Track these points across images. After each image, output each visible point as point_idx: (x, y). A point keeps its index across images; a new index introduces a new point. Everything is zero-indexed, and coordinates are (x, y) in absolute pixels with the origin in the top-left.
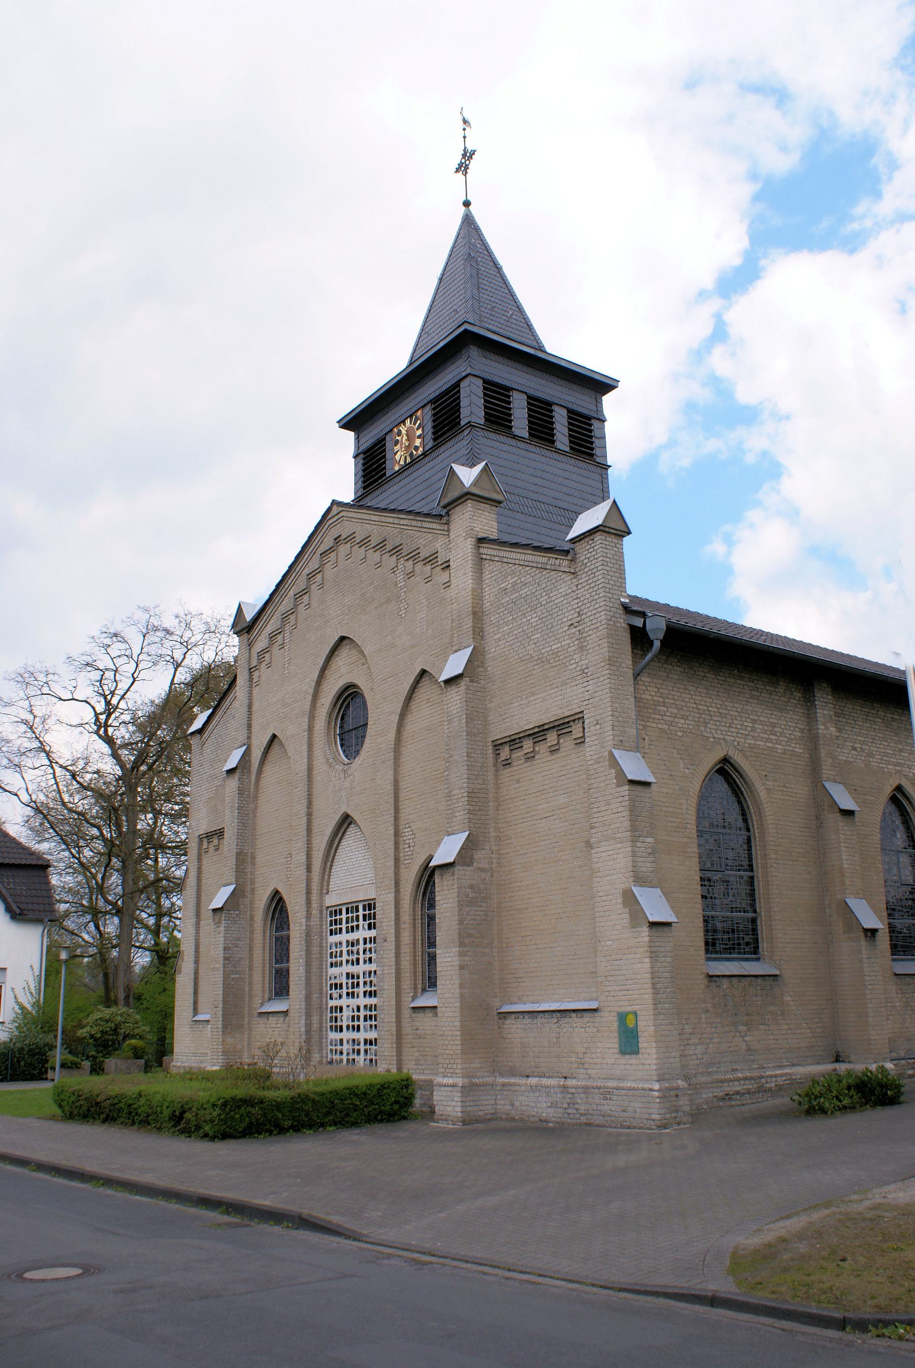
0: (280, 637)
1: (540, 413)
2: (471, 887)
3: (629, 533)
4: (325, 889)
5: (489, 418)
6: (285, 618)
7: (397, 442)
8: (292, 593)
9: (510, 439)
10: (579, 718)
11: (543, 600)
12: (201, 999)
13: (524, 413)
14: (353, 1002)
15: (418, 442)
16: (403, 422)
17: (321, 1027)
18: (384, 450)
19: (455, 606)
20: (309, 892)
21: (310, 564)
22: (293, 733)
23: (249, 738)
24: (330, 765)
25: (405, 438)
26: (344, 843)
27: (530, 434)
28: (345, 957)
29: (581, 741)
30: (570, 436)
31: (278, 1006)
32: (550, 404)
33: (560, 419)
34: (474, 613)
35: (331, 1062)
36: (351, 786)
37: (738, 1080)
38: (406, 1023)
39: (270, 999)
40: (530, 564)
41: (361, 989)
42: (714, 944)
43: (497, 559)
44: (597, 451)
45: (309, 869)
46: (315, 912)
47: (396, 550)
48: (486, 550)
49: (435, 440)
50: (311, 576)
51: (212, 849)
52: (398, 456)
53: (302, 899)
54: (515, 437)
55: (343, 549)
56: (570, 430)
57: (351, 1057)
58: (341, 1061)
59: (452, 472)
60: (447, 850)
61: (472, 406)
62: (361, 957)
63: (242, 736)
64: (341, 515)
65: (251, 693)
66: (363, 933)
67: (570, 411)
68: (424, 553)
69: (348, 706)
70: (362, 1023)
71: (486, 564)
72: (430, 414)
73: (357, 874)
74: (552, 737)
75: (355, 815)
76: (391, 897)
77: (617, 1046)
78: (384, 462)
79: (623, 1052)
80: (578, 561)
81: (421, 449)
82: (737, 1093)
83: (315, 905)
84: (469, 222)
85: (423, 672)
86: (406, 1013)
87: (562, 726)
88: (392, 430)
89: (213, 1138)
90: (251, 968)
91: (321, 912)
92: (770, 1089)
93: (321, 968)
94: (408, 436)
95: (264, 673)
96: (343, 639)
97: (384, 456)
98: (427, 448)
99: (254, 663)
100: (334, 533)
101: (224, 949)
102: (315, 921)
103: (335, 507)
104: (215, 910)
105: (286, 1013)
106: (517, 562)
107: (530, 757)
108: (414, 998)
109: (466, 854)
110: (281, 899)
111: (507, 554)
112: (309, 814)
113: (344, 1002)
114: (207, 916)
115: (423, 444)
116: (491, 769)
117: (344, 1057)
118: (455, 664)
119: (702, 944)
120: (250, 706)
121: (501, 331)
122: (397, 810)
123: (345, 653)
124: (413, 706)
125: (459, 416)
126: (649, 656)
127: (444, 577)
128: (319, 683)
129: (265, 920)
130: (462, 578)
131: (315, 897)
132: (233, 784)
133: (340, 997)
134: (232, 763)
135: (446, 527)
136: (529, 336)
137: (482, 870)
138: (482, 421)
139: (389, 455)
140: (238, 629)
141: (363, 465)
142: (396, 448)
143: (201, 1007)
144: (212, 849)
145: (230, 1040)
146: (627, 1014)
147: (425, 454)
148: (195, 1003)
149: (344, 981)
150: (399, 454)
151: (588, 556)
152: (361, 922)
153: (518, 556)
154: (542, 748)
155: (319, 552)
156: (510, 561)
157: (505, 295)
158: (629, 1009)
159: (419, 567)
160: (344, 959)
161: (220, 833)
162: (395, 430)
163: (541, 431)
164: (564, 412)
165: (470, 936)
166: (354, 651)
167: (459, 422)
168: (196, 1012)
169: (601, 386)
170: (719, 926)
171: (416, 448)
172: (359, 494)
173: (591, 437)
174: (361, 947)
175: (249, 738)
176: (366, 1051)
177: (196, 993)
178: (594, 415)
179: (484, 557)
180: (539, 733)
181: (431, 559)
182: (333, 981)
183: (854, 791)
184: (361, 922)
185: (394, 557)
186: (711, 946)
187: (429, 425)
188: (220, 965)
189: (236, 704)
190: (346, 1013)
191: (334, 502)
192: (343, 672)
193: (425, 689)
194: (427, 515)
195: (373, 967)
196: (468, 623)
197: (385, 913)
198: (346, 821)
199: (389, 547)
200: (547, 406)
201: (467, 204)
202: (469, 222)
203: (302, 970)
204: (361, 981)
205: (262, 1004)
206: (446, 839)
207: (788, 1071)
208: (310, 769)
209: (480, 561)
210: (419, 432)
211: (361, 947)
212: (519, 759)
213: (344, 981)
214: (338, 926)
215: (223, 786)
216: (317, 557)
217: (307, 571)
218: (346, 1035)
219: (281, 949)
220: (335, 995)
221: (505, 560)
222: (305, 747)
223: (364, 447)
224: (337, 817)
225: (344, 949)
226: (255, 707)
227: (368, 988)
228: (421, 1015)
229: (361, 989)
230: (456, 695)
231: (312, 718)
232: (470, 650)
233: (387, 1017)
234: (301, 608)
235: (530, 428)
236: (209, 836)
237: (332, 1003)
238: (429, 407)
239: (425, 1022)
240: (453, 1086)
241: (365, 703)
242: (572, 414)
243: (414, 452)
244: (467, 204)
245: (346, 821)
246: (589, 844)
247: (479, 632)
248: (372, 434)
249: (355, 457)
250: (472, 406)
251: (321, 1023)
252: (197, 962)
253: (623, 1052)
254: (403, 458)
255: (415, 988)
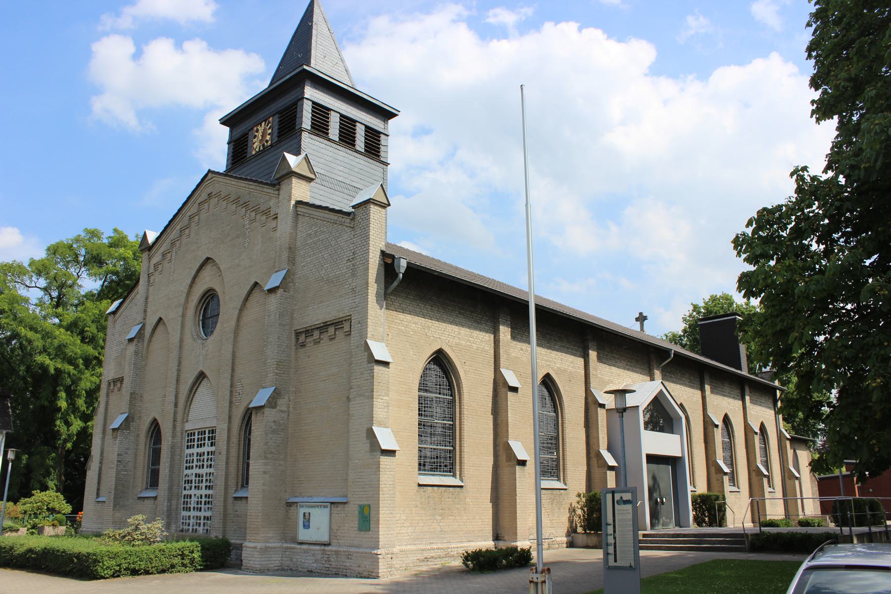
0: (169, 255)
2: (274, 422)
3: (389, 205)
4: (185, 420)
5: (313, 126)
6: (173, 244)
8: (178, 227)
10: (348, 319)
11: (333, 243)
12: (102, 488)
13: (337, 126)
14: (198, 493)
15: (268, 137)
16: (261, 124)
17: (177, 508)
19: (278, 243)
20: (175, 420)
22: (172, 317)
23: (144, 319)
24: (194, 340)
26: (199, 390)
27: (340, 139)
28: (195, 463)
29: (348, 334)
31: (151, 493)
32: (355, 121)
33: (360, 132)
34: (290, 248)
35: (182, 531)
36: (205, 353)
37: (433, 549)
38: (230, 507)
39: (146, 489)
41: (204, 484)
42: (424, 465)
44: (382, 154)
45: (176, 405)
46: (179, 434)
47: (245, 205)
48: (301, 209)
49: (278, 137)
50: (191, 218)
51: (116, 389)
52: (256, 145)
53: (170, 425)
54: (329, 140)
55: (214, 201)
58: (188, 530)
59: (284, 158)
60: (261, 398)
62: (205, 463)
63: (140, 318)
65: (148, 290)
66: (206, 449)
67: (366, 127)
68: (263, 208)
69: (209, 303)
70: (203, 506)
73: (206, 411)
74: (331, 330)
75: (207, 373)
76: (225, 426)
77: (357, 526)
79: (360, 530)
82: (432, 557)
83: (178, 429)
85: (256, 284)
86: (230, 500)
87: (337, 324)
89: (201, 570)
90: (135, 468)
91: (182, 434)
92: (453, 556)
93: (179, 470)
94: (262, 135)
95: (156, 277)
96: (208, 259)
99: (152, 270)
101: (118, 455)
102: (178, 439)
104: (114, 430)
105: (155, 498)
107: (317, 342)
108: (236, 491)
109: (272, 402)
110: (158, 424)
111: (314, 213)
112: (179, 370)
113: (193, 492)
114: (109, 432)
115: (272, 139)
116: (294, 348)
117: (191, 528)
118: (275, 280)
119: (417, 465)
120: (147, 298)
122: (233, 370)
123: (208, 269)
124: (248, 304)
126: (395, 284)
127: (273, 224)
128: (191, 286)
129: (147, 437)
130: (285, 225)
131: (178, 424)
132: (132, 348)
133: (191, 488)
134: (132, 335)
137: (282, 411)
138: (309, 128)
140: (143, 247)
143: (102, 492)
144: (116, 389)
145: (118, 514)
146: (365, 506)
147: (271, 145)
148: (98, 489)
149: (194, 479)
152: (207, 441)
153: (320, 214)
154: (325, 336)
155: (198, 202)
158: (366, 503)
159: (258, 216)
160: (194, 464)
161: (121, 380)
164: (363, 127)
165: (271, 453)
166: (215, 267)
168: (98, 495)
170: (428, 454)
171: (267, 141)
174: (206, 457)
175: (144, 319)
176: (204, 524)
177: (99, 483)
180: (324, 327)
181: (266, 212)
182: (187, 478)
183: (519, 375)
184: (207, 441)
186: (422, 466)
187: (276, 128)
188: (114, 466)
189: (138, 296)
190: (194, 499)
191: (209, 171)
192: (207, 280)
193: (256, 294)
195: (211, 470)
196: (285, 255)
197: (221, 437)
198: (202, 376)
199: (241, 202)
200: (353, 122)
203: (167, 471)
204: (204, 479)
205: (141, 492)
206: (261, 390)
207: (465, 544)
208: (181, 341)
209: (297, 215)
210: (270, 131)
211: (206, 457)
212: (310, 342)
213: (194, 479)
215: (126, 349)
217: (189, 214)
218: (193, 513)
219: (155, 456)
220: (187, 488)
222: (179, 327)
224: (196, 373)
225: (195, 458)
226: (150, 299)
227: (208, 484)
228: (239, 502)
229: (204, 484)
230: (273, 300)
231: (185, 308)
232: (285, 271)
233: (218, 503)
234: (184, 237)
236: (115, 381)
237: (185, 493)
239: (240, 505)
240: (255, 548)
241: (219, 301)
245: (202, 376)
246: (348, 399)
247: (292, 261)
248: (241, 130)
251: (177, 504)
252: (101, 463)
253: (360, 530)
255: (237, 485)
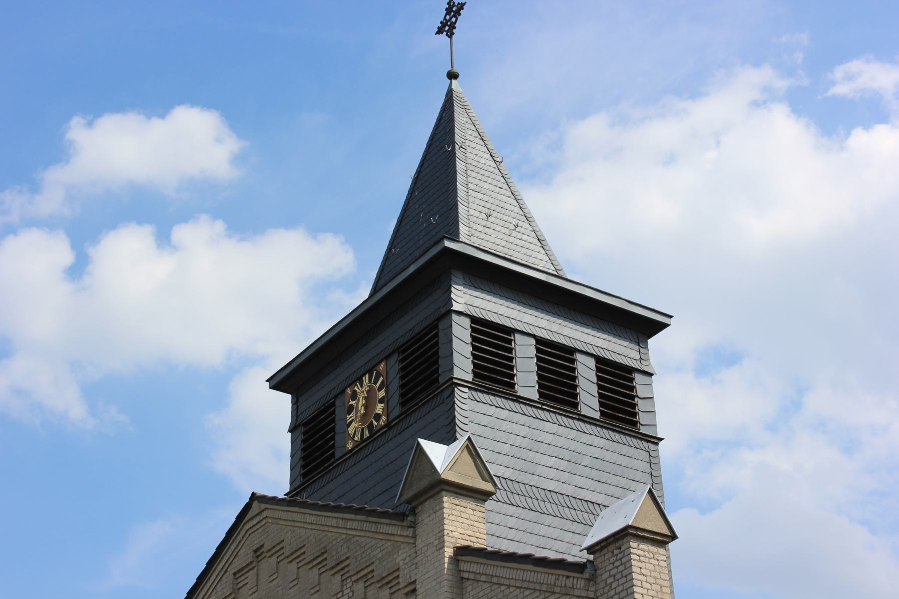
1: (556, 361)
7: (350, 409)
9: (511, 403)
15: (379, 408)
18: (333, 421)
21: (219, 588)
25: (362, 402)
27: (541, 395)
30: (601, 396)
32: (572, 351)
33: (525, 355)
40: (531, 586)
43: (483, 578)
44: (642, 418)
47: (340, 567)
49: (403, 404)
54: (518, 399)
55: (267, 565)
56: (600, 387)
64: (264, 514)
68: (380, 571)
71: (469, 586)
72: (397, 367)
78: (333, 438)
80: (599, 580)
81: (384, 418)
88: (343, 391)
94: (366, 403)
97: (333, 429)
98: (392, 417)
100: (254, 541)
103: (255, 504)
106: (512, 583)
121: (500, 249)
125: (437, 370)
135: (410, 532)
136: (540, 256)
138: (470, 377)
139: (339, 427)
141: (304, 441)
142: (349, 418)
147: (388, 426)
150: (354, 425)
151: (614, 572)
153: (514, 574)
156: (502, 581)
157: (505, 199)
162: (349, 391)
163: (557, 390)
164: (591, 362)
167: (437, 380)
171: (378, 417)
172: (297, 483)
173: (633, 397)
178: (635, 365)
179: (466, 575)
185: (338, 578)
187: (395, 384)
191: (254, 497)
194: (384, 515)
199: (331, 563)
210: (382, 394)
216: (228, 578)
221: (495, 580)
223: (303, 417)
235: (540, 386)
238: (395, 358)
242: (604, 365)
243: (375, 423)
249: (291, 430)
254: (359, 430)
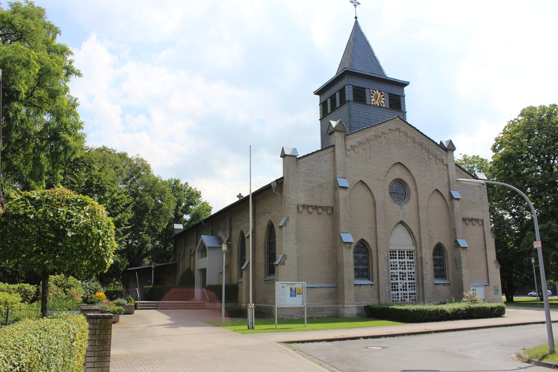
57: (403, 299)
58: (398, 300)
61: (349, 95)
84: (356, 25)
169: (403, 85)
182: (392, 274)
201: (356, 18)
202: (356, 26)
214: (397, 257)
227: (410, 277)
244: (356, 18)
250: (349, 95)
